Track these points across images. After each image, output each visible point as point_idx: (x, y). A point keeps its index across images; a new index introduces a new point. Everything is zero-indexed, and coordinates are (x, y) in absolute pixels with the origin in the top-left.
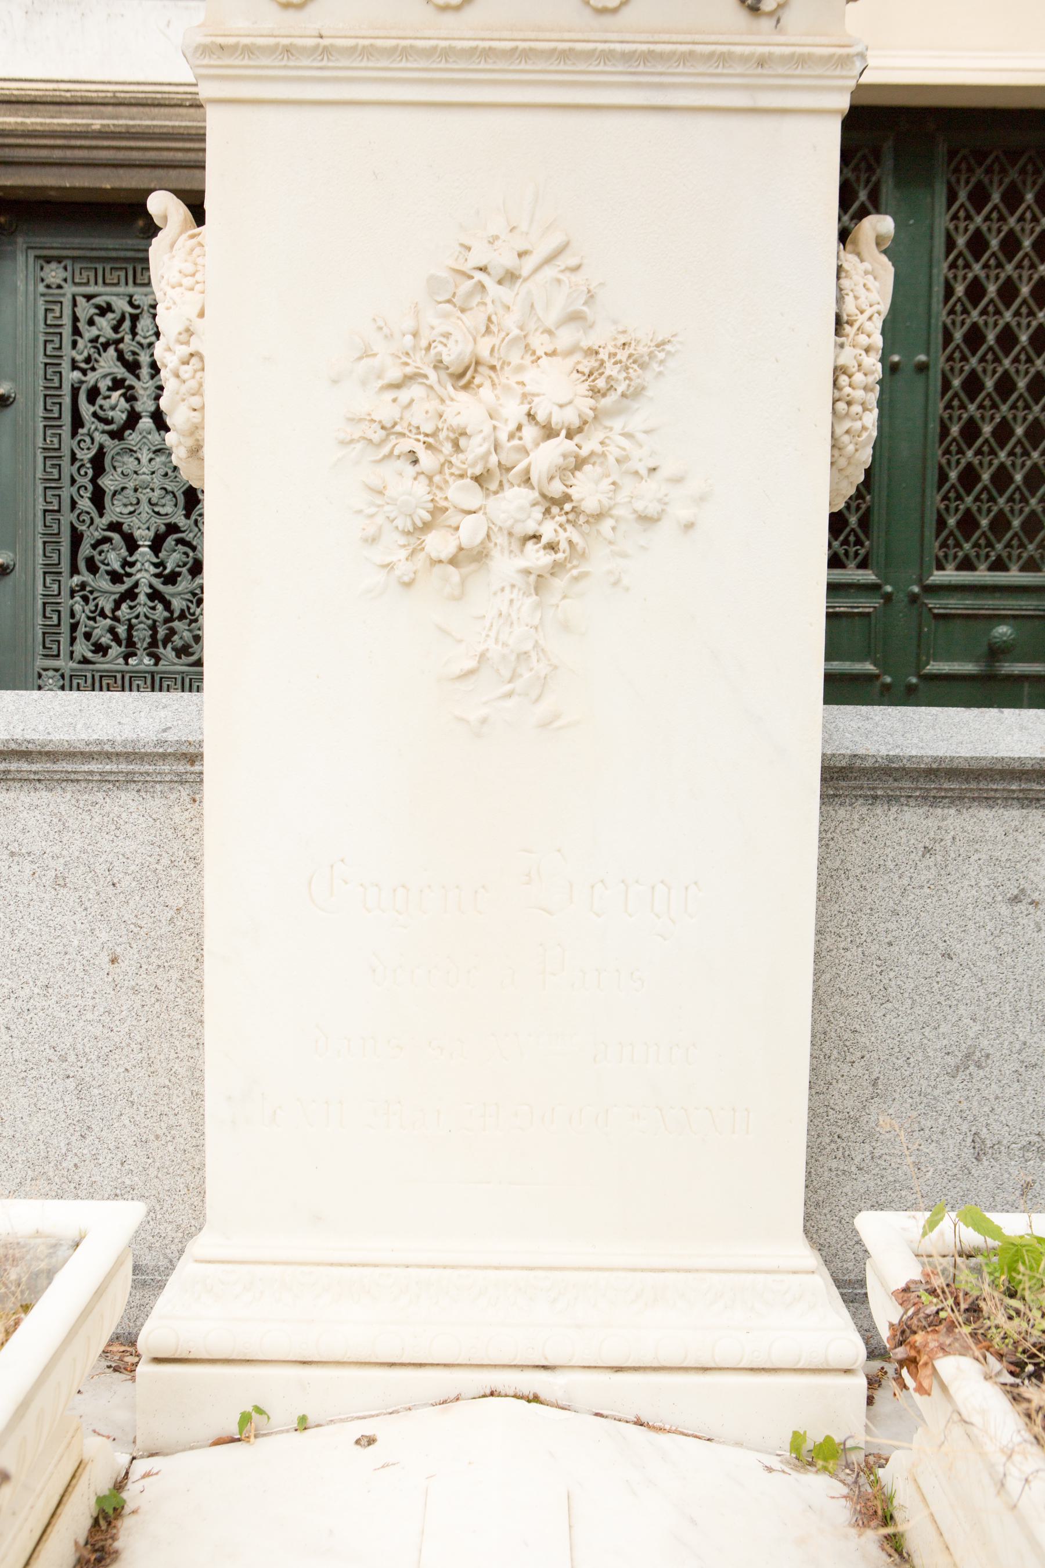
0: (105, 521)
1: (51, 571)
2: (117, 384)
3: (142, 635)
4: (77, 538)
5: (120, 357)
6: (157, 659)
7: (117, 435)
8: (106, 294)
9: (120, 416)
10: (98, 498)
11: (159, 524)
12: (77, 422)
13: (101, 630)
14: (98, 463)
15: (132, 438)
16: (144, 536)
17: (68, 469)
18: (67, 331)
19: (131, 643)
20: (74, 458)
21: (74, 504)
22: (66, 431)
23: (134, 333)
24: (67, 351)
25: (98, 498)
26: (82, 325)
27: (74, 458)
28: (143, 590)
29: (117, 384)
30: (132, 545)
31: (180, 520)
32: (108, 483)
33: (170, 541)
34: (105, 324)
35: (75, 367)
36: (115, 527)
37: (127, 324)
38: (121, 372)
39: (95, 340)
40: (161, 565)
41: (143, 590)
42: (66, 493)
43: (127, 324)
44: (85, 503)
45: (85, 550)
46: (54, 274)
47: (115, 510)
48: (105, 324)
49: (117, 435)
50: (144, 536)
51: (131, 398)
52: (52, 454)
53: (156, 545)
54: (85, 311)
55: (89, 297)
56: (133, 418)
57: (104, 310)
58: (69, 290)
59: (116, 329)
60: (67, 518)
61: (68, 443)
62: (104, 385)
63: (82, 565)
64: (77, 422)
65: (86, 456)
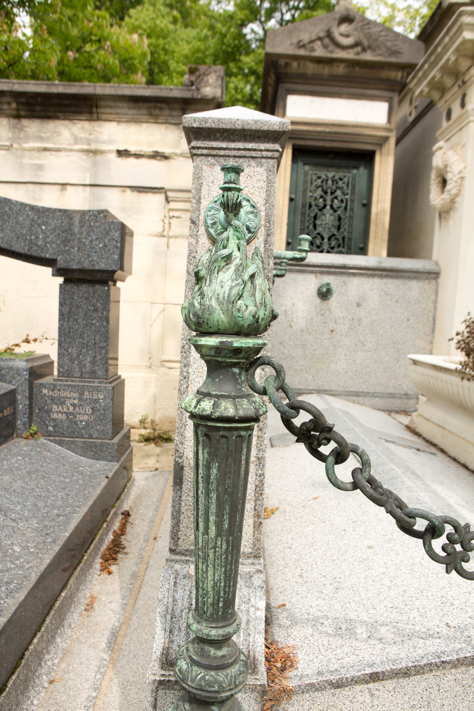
0: (316, 232)
1: (352, 201)
2: (321, 197)
3: (330, 182)
4: (346, 208)
5: (323, 190)
6: (326, 176)
7: (321, 210)
8: (320, 174)
9: (321, 205)
10: (315, 226)
11: (330, 234)
12: (343, 238)
13: (340, 184)
14: (315, 218)
15: (325, 211)
16: (326, 236)
17: (307, 218)
18: (309, 183)
19: (333, 181)
20: (309, 215)
21: (308, 227)
22: (307, 208)
23: (326, 184)
24: (309, 188)
25: (315, 226)
26: (313, 181)
27: (309, 215)
28: (329, 194)
29: (321, 197)
30: (323, 238)
31: (335, 232)
32: (318, 222)
33: (333, 238)
34: (319, 181)
35: (311, 191)
36: (319, 234)
37: (325, 182)
38: (322, 194)
39: (316, 186)
40: (330, 244)
41: (329, 194)
42: (307, 224)
43: (325, 182)
44: (311, 227)
45: (344, 205)
46: (307, 168)
47: (319, 229)
48: (319, 181)
49: (321, 210)
50: (326, 236)
51: (325, 200)
52: (303, 214)
53: (329, 239)
54: (314, 177)
55: (316, 174)
56: (325, 206)
57: (319, 178)
58: (311, 172)
59: (322, 182)
60: (348, 214)
61: (308, 212)
62: (318, 197)
63: (345, 201)
64: (343, 238)
65: (313, 215)
